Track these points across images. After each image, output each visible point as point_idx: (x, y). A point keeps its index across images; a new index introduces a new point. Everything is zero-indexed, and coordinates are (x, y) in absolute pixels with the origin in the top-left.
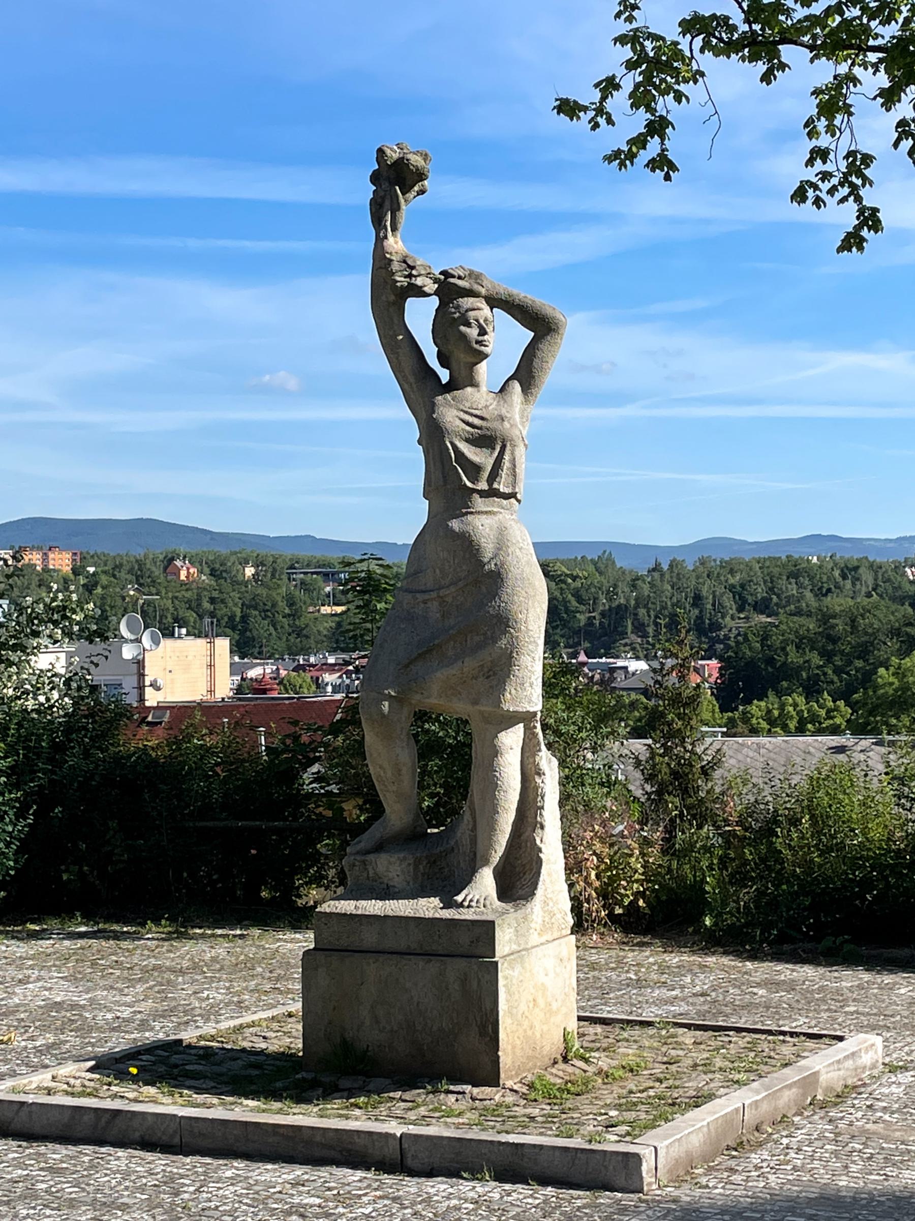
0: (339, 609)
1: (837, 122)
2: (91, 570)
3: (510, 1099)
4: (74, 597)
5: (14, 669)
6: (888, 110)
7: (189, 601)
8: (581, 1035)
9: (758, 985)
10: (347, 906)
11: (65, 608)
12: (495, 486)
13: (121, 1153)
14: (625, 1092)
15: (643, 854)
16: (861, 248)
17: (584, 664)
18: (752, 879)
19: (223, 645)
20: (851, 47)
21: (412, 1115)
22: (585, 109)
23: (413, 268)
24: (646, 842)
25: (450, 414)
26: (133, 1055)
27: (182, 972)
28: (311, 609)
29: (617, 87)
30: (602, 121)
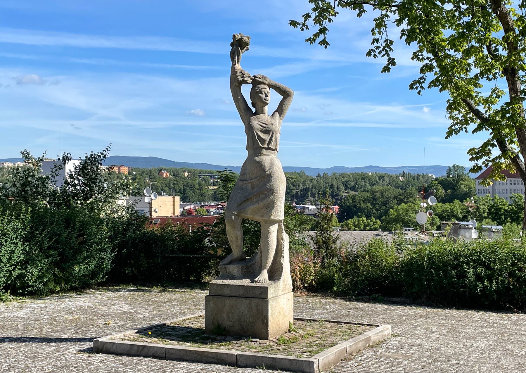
0: (215, 187)
1: (382, 30)
2: (134, 173)
3: (272, 344)
4: (131, 181)
5: (110, 204)
6: (398, 26)
7: (166, 184)
8: (295, 324)
9: (351, 309)
10: (220, 282)
11: (127, 184)
13: (146, 359)
14: (308, 342)
15: (314, 267)
16: (389, 71)
17: (295, 206)
18: (349, 275)
19: (178, 198)
20: (386, 5)
21: (240, 348)
22: (299, 24)
24: (315, 263)
25: (255, 122)
26: (150, 328)
27: (165, 302)
28: (206, 187)
29: (310, 17)
30: (304, 28)
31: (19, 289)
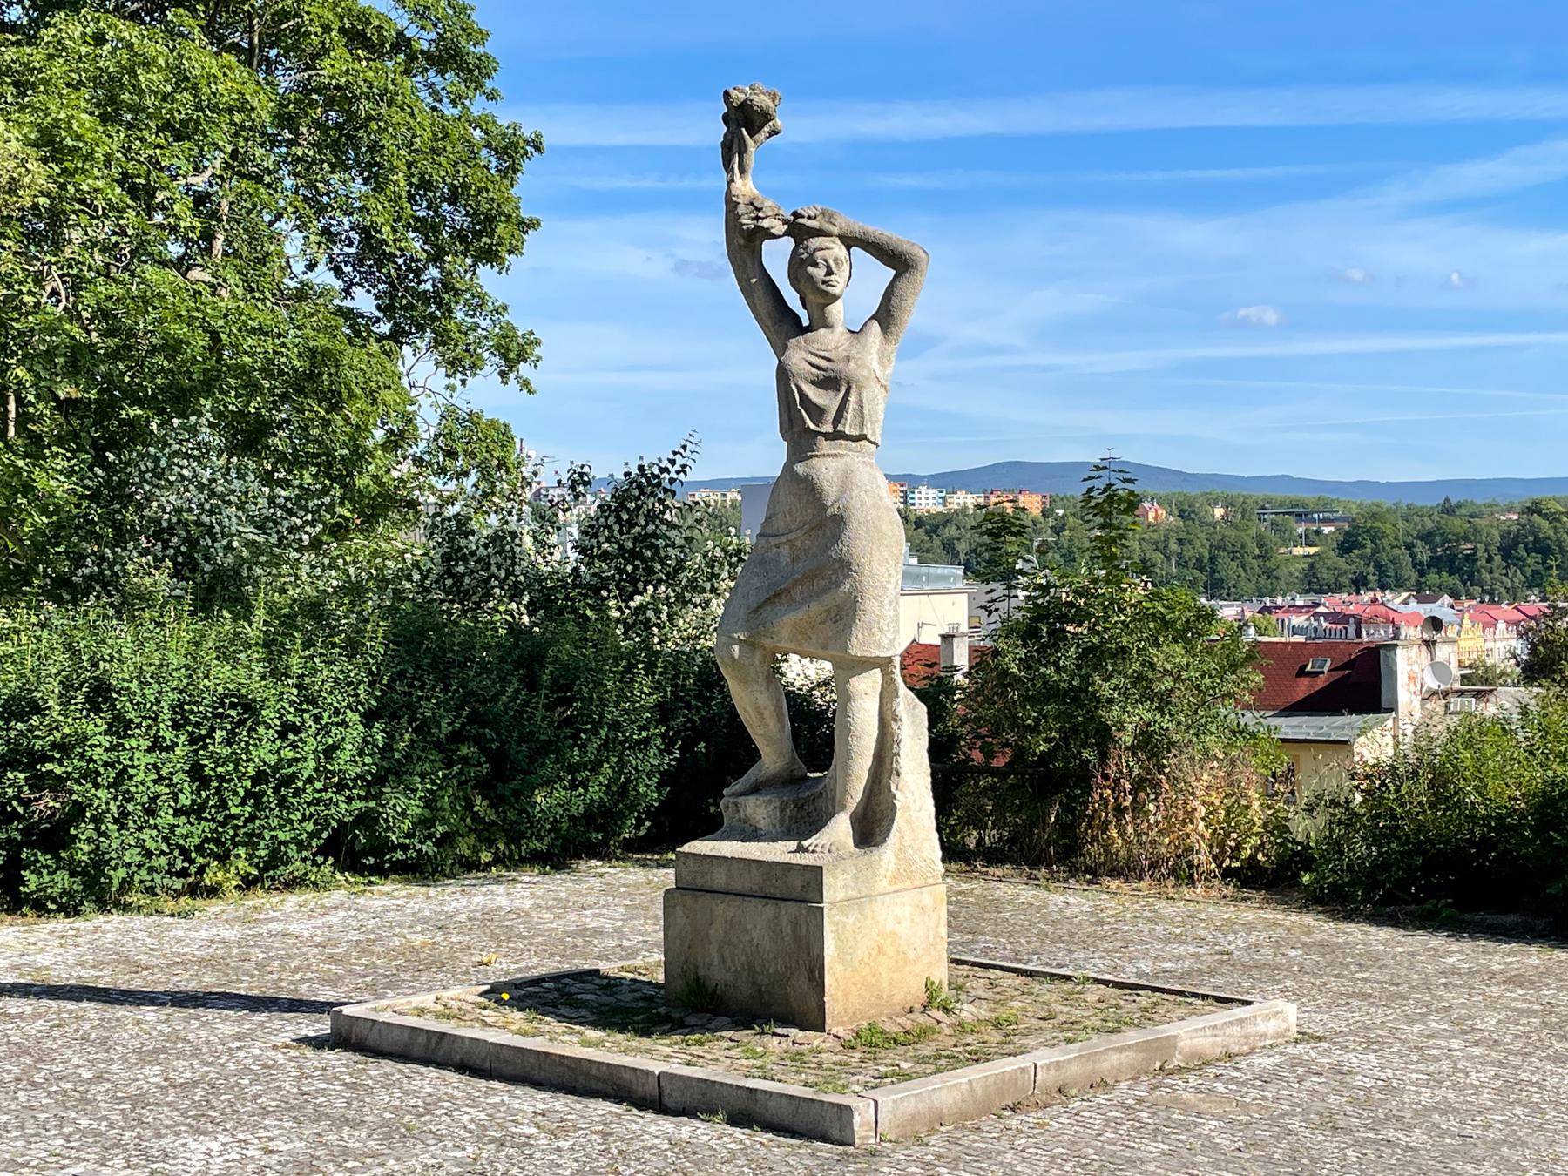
0: (1312, 550)
2: (1061, 512)
12: (840, 428)
23: (760, 210)
25: (799, 357)
28: (1283, 550)
31: (366, 855)
